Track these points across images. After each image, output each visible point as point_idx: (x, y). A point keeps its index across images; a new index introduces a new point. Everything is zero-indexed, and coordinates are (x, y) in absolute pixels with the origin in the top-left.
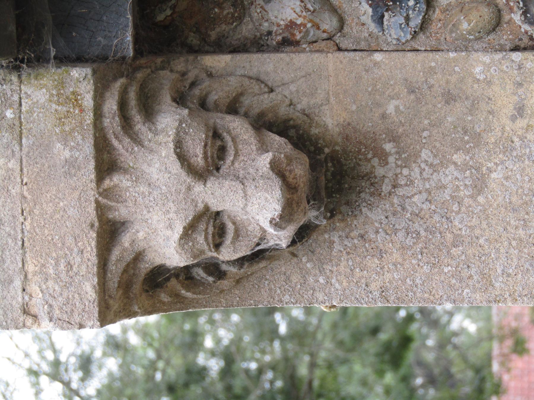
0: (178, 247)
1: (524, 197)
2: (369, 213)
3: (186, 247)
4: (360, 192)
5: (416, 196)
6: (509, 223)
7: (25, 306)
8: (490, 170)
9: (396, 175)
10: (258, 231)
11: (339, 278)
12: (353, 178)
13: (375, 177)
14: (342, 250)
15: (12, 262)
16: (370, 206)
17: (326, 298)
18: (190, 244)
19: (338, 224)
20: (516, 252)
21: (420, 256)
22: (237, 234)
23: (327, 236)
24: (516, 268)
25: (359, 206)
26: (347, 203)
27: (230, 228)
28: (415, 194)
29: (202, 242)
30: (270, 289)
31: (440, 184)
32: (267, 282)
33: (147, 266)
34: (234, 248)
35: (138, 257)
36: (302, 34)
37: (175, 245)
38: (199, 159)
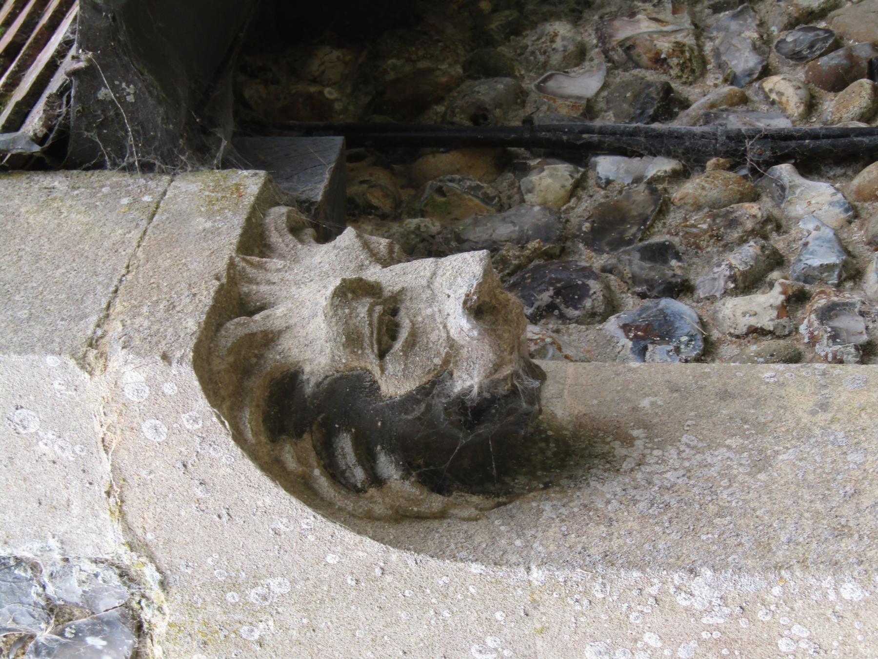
0: (329, 307)
1: (824, 476)
2: (599, 486)
3: (340, 312)
4: (589, 468)
5: (670, 473)
6: (802, 498)
7: (94, 342)
8: (777, 453)
9: (644, 456)
10: (444, 345)
11: (544, 542)
12: (582, 457)
13: (614, 456)
14: (554, 517)
15: (94, 303)
16: (603, 481)
17: (521, 560)
18: (347, 311)
19: (553, 495)
20: (810, 522)
21: (667, 525)
22: (412, 343)
23: (534, 504)
24: (808, 537)
25: (586, 479)
26: (570, 477)
27: (404, 334)
28: (668, 471)
29: (362, 315)
30: (441, 543)
31: (705, 463)
32: (437, 535)
33: (278, 357)
34: (405, 365)
35: (269, 339)
36: (537, 347)
37: (325, 303)
38: (381, 247)
